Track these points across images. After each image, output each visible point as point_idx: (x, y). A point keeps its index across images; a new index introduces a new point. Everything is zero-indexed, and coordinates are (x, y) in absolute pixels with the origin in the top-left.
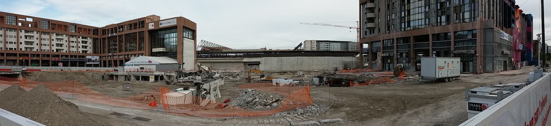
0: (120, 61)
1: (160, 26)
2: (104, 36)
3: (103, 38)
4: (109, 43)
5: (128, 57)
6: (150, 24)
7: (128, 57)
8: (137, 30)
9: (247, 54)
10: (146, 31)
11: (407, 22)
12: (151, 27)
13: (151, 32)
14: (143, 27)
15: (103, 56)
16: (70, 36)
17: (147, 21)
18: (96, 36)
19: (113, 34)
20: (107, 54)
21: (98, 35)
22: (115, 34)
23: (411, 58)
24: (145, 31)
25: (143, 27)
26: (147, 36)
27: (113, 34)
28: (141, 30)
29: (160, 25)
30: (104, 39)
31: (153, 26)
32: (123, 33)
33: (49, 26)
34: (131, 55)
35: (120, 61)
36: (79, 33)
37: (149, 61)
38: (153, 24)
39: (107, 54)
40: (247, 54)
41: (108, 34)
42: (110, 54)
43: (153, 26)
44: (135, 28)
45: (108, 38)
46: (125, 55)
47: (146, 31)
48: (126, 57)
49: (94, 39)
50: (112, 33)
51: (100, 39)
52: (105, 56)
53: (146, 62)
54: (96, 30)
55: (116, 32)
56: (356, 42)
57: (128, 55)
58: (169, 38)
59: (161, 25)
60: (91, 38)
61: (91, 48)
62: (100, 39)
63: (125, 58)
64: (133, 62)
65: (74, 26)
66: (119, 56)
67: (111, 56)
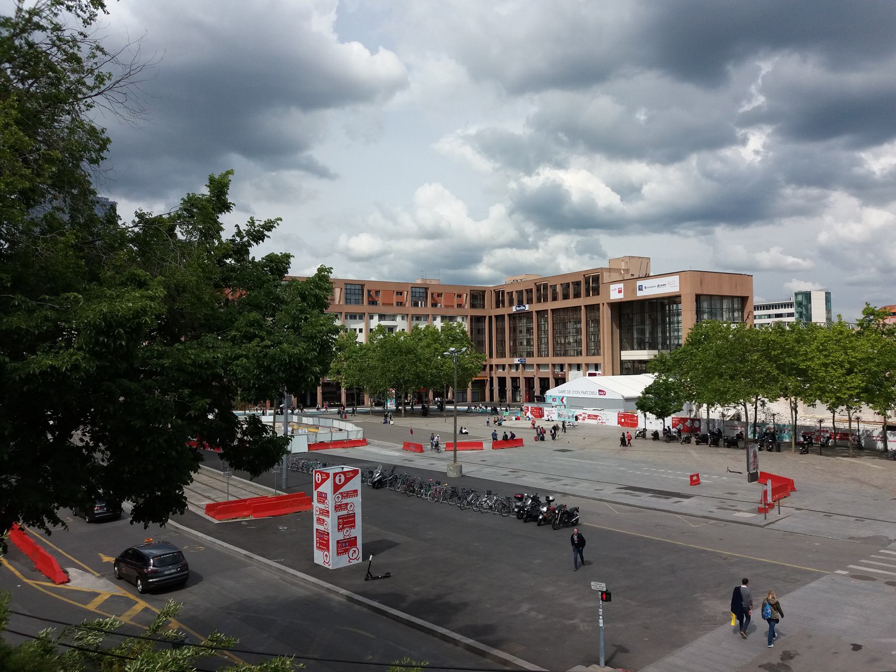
0: (541, 379)
1: (640, 294)
2: (500, 311)
3: (497, 317)
4: (513, 330)
5: (562, 370)
6: (612, 287)
7: (562, 370)
8: (582, 302)
10: (603, 304)
12: (616, 293)
13: (618, 308)
14: (596, 291)
15: (497, 366)
16: (412, 317)
17: (606, 278)
18: (478, 312)
19: (522, 308)
20: (506, 361)
21: (484, 307)
22: (527, 306)
24: (601, 306)
26: (605, 315)
27: (522, 308)
28: (592, 300)
29: (640, 290)
30: (500, 318)
31: (620, 292)
34: (570, 365)
35: (541, 379)
36: (434, 309)
37: (599, 391)
38: (621, 285)
39: (506, 361)
41: (511, 304)
42: (516, 361)
43: (620, 292)
44: (577, 295)
45: (509, 315)
46: (554, 365)
47: (603, 304)
48: (557, 370)
50: (520, 303)
51: (490, 317)
52: (504, 367)
53: (593, 393)
54: (477, 297)
55: (530, 301)
57: (562, 367)
59: (641, 289)
60: (464, 317)
62: (490, 317)
63: (553, 373)
64: (564, 392)
65: (422, 290)
66: (538, 365)
67: (517, 366)
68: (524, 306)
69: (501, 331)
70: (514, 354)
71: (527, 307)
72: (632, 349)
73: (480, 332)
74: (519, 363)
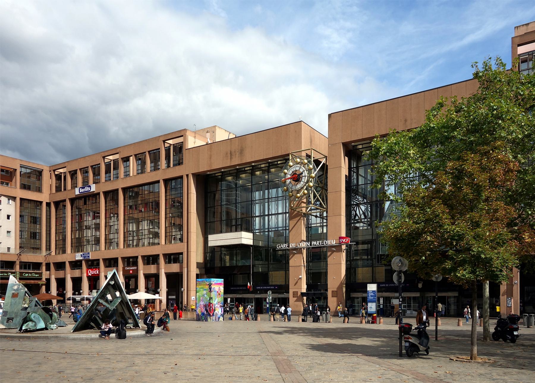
2: (60, 197)
4: (78, 219)
9: (275, 287)
10: (187, 175)
11: (57, 336)
14: (179, 163)
19: (87, 189)
21: (39, 190)
23: (372, 266)
25: (179, 163)
27: (87, 189)
32: (120, 184)
33: (86, 191)
40: (275, 287)
41: (74, 186)
42: (78, 257)
47: (187, 175)
49: (26, 204)
56: (336, 291)
58: (268, 198)
61: (13, 234)
68: (90, 186)
69: (61, 221)
70: (78, 245)
71: (94, 188)
72: (221, 232)
73: (35, 220)
74: (82, 258)
